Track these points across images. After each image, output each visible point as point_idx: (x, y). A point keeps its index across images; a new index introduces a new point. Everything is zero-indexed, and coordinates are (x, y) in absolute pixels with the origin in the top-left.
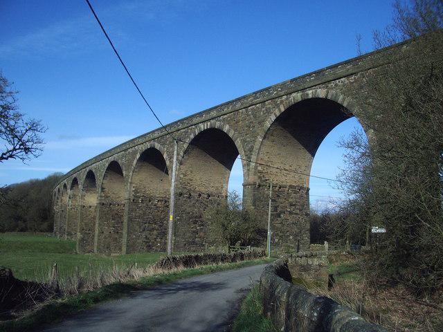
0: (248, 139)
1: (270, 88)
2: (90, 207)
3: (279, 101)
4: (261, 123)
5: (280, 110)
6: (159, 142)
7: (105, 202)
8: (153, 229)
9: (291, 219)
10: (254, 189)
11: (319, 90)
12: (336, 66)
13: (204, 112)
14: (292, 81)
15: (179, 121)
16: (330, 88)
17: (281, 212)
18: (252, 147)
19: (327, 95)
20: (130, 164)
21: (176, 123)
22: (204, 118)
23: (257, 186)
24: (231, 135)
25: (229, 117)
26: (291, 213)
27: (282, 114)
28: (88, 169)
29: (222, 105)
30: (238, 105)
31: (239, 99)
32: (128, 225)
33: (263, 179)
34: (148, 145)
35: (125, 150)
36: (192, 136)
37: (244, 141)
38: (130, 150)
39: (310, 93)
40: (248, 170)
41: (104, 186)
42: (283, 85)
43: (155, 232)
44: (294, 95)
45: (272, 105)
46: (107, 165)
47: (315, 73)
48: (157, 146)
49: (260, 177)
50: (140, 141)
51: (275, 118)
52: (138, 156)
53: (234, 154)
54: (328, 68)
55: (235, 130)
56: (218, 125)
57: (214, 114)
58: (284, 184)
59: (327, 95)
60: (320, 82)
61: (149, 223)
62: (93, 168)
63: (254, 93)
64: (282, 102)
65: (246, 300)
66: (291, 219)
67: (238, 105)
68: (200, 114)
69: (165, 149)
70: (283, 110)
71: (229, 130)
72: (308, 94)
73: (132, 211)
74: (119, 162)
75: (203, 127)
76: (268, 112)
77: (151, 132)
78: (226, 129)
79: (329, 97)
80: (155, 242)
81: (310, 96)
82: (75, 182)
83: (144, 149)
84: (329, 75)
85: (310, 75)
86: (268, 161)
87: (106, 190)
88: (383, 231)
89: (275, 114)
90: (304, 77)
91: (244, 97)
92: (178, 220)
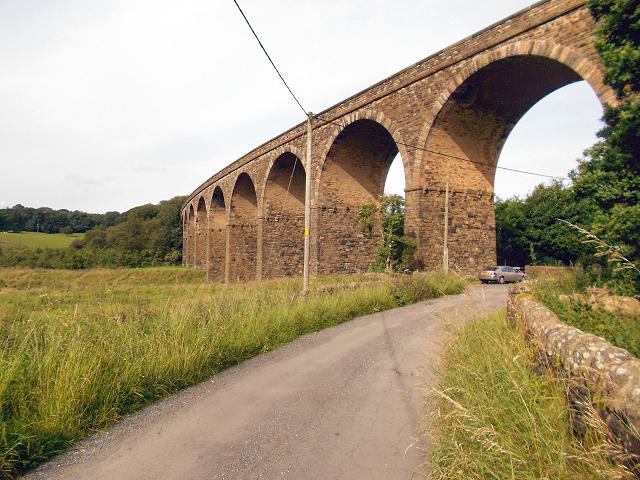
3: (453, 69)
4: (428, 105)
5: (456, 82)
6: (296, 145)
8: (294, 253)
9: (470, 235)
13: (351, 98)
16: (536, 38)
18: (417, 139)
20: (263, 176)
24: (386, 126)
26: (469, 227)
29: (373, 87)
30: (396, 85)
31: (397, 75)
34: (282, 150)
37: (405, 132)
39: (503, 51)
40: (412, 170)
41: (234, 204)
47: (512, 17)
49: (427, 180)
50: (273, 145)
51: (449, 95)
52: (271, 164)
54: (533, 7)
57: (363, 100)
58: (461, 187)
60: (520, 30)
64: (459, 70)
72: (499, 54)
74: (250, 173)
75: (349, 119)
76: (439, 87)
79: (535, 52)
83: (278, 155)
85: (503, 22)
90: (492, 28)
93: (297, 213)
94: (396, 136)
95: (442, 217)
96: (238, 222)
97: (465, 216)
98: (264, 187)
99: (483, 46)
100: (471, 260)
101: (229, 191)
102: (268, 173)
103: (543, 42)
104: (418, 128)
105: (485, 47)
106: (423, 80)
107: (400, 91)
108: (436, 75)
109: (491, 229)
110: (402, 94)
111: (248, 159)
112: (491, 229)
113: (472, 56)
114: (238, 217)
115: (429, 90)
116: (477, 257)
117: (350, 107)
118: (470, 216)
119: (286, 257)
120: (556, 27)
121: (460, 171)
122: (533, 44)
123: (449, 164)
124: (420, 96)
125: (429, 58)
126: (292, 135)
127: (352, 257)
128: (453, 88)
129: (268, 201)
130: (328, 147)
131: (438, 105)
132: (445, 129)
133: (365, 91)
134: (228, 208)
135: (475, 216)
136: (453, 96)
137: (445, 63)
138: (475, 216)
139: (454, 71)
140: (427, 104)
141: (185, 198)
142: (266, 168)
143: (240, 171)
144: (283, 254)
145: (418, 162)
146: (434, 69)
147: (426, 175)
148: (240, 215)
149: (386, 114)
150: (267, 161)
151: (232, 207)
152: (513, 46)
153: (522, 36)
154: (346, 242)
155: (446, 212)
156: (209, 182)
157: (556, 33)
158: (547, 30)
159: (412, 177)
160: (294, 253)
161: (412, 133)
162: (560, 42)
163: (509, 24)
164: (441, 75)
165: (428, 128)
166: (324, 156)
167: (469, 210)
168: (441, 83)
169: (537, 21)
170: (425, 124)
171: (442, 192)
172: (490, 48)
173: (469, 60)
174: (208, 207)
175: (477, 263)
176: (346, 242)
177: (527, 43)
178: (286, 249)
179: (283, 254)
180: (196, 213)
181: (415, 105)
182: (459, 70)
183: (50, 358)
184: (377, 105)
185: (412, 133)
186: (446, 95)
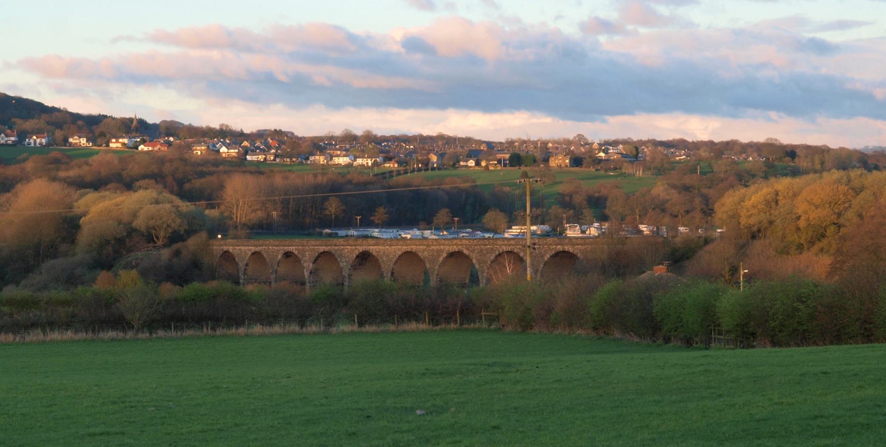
4: (543, 256)
5: (552, 252)
69: (474, 256)
70: (553, 253)
83: (451, 251)
129: (439, 276)
186: (548, 256)
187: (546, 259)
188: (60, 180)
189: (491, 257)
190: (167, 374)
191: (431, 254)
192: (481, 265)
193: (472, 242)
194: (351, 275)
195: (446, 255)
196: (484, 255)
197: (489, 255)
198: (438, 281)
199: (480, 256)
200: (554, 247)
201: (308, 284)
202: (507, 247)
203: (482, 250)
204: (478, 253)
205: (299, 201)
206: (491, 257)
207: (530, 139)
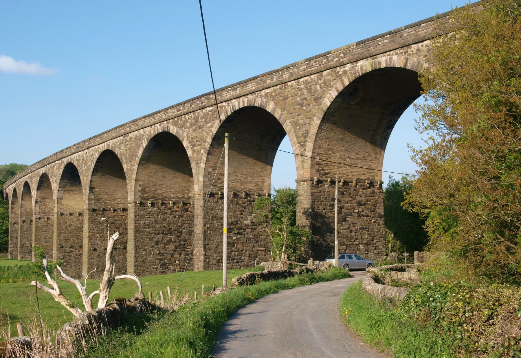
0: (301, 122)
1: (329, 53)
2: (71, 214)
3: (340, 70)
4: (318, 100)
5: (343, 83)
6: (176, 124)
7: (96, 208)
8: (169, 241)
9: (360, 223)
10: (312, 187)
11: (395, 58)
12: (418, 24)
13: (240, 83)
14: (358, 44)
15: (203, 96)
16: (410, 55)
17: (346, 215)
18: (307, 132)
19: (406, 64)
20: (133, 155)
21: (199, 98)
22: (239, 91)
23: (315, 183)
24: (277, 116)
25: (275, 91)
26: (359, 215)
27: (346, 88)
28: (65, 161)
29: (263, 75)
30: (286, 76)
31: (287, 68)
32: (136, 238)
33: (322, 172)
34: (159, 129)
35: (125, 135)
36: (223, 117)
37: (295, 124)
38: (131, 135)
39: (383, 61)
40: (303, 162)
41: (94, 184)
42: (346, 51)
43: (172, 246)
44: (360, 63)
45: (332, 76)
46: (97, 156)
47: (390, 33)
48: (173, 130)
49: (318, 171)
50: (147, 121)
51: (336, 94)
52: (145, 144)
53: (281, 134)
54: (406, 27)
55: (283, 109)
56: (258, 103)
57: (252, 86)
58: (350, 177)
59: (406, 64)
60: (396, 46)
61: (163, 233)
62: (74, 158)
63: (306, 60)
64: (345, 72)
65: (345, 106)
66: (360, 223)
67: (286, 76)
68: (233, 87)
69: (185, 134)
70: (347, 83)
71: (275, 109)
72: (380, 63)
73: (140, 218)
74: (117, 151)
75: (237, 104)
76: (327, 85)
77: (162, 110)
78: (270, 108)
79: (409, 67)
80: (173, 260)
81: (383, 65)
82: (44, 181)
83: (153, 134)
84: (408, 35)
85: (382, 36)
86: (328, 149)
87: (97, 190)
88: (168, 288)
89: (336, 89)
90: (374, 39)
91: (294, 65)
92: (208, 228)
93: (172, 196)
94: (287, 126)
95: (333, 206)
96: (99, 206)
97: (355, 204)
98: (135, 167)
99: (366, 54)
100: (361, 247)
101: (87, 170)
102: (140, 152)
103: (415, 59)
104: (307, 121)
105: (368, 55)
106: (312, 76)
107: (289, 84)
108: (325, 73)
109: (380, 216)
110: (291, 86)
111: (114, 135)
112: (380, 216)
113: (357, 61)
114: (97, 200)
115: (318, 86)
116: (367, 244)
117: (238, 92)
118: (360, 204)
119: (161, 246)
120: (424, 48)
121: (348, 161)
122: (407, 60)
123: (338, 155)
124: (309, 90)
125: (317, 57)
126: (171, 113)
127: (239, 246)
128: (341, 88)
129: (140, 183)
130: (214, 130)
131: (327, 102)
132: (334, 123)
133: (255, 78)
134: (86, 190)
135: (365, 205)
136: (341, 95)
137: (332, 64)
138: (365, 205)
139: (341, 73)
140: (316, 100)
141: (23, 168)
142: (138, 146)
143: (103, 147)
144: (157, 243)
145: (309, 154)
146: (322, 67)
147: (317, 167)
148: (100, 197)
149: (276, 104)
150: (139, 139)
151: (91, 188)
152: (391, 58)
153: (398, 51)
154: (233, 229)
155: (336, 201)
156: (58, 156)
157: (425, 53)
158: (418, 50)
159: (303, 168)
160: (169, 241)
161: (302, 125)
162: (429, 61)
163: (387, 39)
164: (328, 75)
165: (318, 122)
166: (209, 140)
167: (358, 198)
168: (329, 81)
169: (410, 40)
170: (315, 118)
171: (333, 182)
172: (373, 56)
173: (354, 64)
174: (55, 186)
175: (367, 250)
176: (233, 229)
177: (403, 58)
178: (160, 237)
179: (157, 243)
180: (34, 192)
181: (305, 99)
182: (345, 72)
183: (385, 41)
184: (267, 95)
185: (302, 125)
186: (334, 94)
187: (329, 104)
188: (4, 208)
189: (213, 129)
190: (67, 332)
191: (128, 146)
192: (195, 148)
193: (181, 108)
194: (62, 199)
195: (147, 143)
196: (200, 127)
197: (210, 124)
198: (139, 191)
199: (195, 130)
200: (348, 67)
201: (34, 215)
202: (241, 100)
203: (196, 120)
204: (192, 125)
205: (171, 324)
206: (213, 129)
207: (250, 105)
